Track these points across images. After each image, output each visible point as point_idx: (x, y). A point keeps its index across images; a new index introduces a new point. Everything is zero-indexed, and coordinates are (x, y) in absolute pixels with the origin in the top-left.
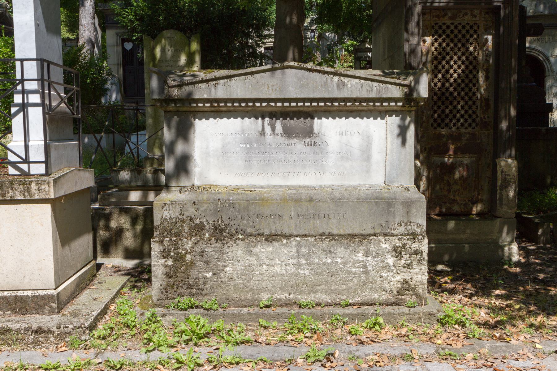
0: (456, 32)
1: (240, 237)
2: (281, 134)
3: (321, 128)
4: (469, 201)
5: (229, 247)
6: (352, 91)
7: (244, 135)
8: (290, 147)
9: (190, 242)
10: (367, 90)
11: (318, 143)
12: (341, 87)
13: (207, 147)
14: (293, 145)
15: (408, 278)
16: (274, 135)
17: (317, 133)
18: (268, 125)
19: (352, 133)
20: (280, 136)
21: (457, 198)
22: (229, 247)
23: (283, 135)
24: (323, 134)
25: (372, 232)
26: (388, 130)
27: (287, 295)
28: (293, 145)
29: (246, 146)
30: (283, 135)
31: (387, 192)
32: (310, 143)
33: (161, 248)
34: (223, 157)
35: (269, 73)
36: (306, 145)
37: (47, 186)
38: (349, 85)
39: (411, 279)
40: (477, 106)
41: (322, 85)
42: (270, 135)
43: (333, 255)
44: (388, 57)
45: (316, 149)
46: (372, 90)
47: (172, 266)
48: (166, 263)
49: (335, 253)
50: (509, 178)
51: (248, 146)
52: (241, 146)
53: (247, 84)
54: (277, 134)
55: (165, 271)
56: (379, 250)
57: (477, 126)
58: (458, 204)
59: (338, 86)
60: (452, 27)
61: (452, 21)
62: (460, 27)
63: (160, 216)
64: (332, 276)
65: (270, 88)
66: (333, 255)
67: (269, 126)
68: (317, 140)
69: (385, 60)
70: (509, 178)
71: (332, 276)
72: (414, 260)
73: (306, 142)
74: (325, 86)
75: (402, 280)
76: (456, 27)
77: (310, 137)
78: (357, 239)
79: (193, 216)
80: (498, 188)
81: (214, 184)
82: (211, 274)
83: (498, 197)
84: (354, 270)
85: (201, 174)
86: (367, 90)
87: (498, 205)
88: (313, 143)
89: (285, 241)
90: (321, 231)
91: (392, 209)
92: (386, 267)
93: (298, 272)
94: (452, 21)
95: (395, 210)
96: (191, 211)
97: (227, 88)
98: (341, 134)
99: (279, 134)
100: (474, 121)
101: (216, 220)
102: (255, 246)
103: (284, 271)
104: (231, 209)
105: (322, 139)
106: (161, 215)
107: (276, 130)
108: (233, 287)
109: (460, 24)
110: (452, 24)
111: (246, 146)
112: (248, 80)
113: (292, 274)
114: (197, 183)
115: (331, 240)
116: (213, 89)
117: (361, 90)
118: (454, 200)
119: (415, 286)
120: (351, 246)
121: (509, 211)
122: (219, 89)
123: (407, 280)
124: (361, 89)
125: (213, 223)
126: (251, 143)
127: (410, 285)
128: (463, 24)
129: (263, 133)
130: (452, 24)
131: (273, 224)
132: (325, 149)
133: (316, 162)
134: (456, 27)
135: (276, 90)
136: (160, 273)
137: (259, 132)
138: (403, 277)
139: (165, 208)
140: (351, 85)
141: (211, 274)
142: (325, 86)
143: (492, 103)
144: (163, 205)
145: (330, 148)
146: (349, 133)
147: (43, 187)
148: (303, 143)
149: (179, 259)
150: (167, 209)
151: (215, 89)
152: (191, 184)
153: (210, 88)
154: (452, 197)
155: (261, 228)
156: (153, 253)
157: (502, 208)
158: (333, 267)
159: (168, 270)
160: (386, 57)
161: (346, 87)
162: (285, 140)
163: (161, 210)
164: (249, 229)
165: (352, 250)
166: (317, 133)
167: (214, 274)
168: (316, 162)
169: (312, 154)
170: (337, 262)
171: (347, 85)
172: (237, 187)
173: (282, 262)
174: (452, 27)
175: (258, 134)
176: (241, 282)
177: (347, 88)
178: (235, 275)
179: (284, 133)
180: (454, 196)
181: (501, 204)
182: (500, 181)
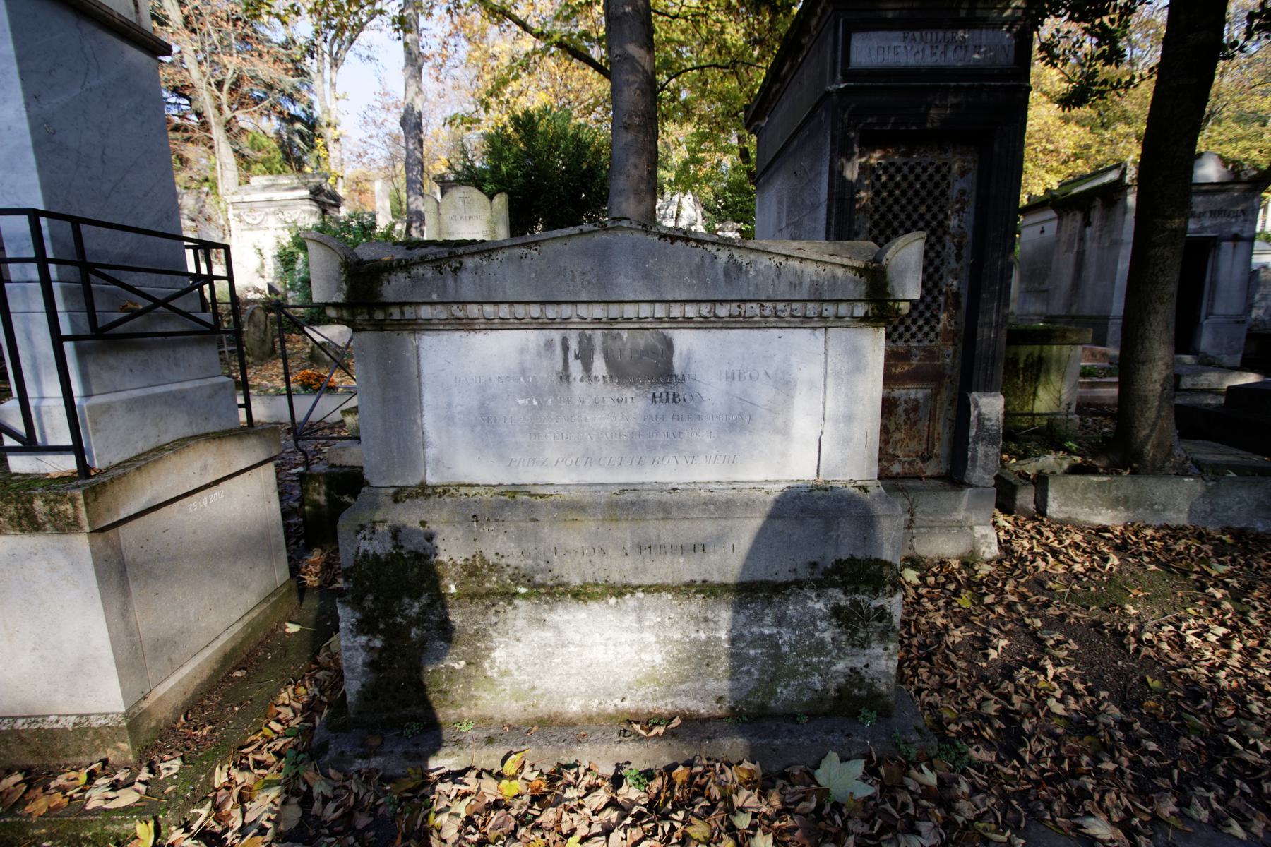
0: (911, 177)
1: (523, 590)
2: (604, 377)
3: (688, 364)
4: (917, 456)
5: (498, 612)
6: (757, 285)
7: (525, 379)
8: (623, 405)
9: (416, 604)
10: (791, 283)
11: (681, 397)
12: (734, 275)
13: (450, 405)
14: (629, 400)
15: (860, 666)
16: (590, 380)
17: (680, 376)
18: (577, 357)
19: (754, 374)
20: (601, 382)
21: (899, 453)
22: (498, 612)
23: (607, 379)
24: (693, 376)
25: (791, 577)
26: (829, 368)
27: (618, 701)
28: (629, 400)
29: (531, 402)
30: (607, 379)
31: (824, 496)
32: (664, 396)
33: (358, 615)
34: (483, 426)
35: (1085, 314)
36: (657, 400)
37: (69, 506)
38: (752, 273)
39: (867, 666)
40: (939, 305)
41: (691, 272)
42: (582, 380)
43: (712, 625)
44: (788, 225)
45: (678, 408)
46: (801, 284)
47: (382, 650)
48: (371, 644)
49: (715, 622)
50: (989, 423)
51: (535, 403)
52: (521, 402)
53: (526, 269)
54: (596, 377)
55: (368, 659)
56: (804, 614)
57: (937, 337)
58: (900, 461)
59: (727, 273)
60: (906, 169)
61: (906, 160)
62: (918, 170)
63: (353, 551)
64: (708, 665)
65: (577, 280)
66: (712, 625)
67: (579, 361)
68: (681, 391)
69: (781, 230)
70: (989, 423)
71: (708, 665)
72: (873, 633)
73: (658, 394)
74: (698, 273)
75: (848, 671)
76: (912, 170)
77: (664, 384)
78: (761, 595)
79: (421, 550)
80: (971, 440)
81: (467, 481)
82: (463, 663)
83: (970, 454)
84: (752, 652)
85: (438, 461)
86: (791, 283)
87: (969, 467)
88: (671, 396)
89: (613, 601)
90: (687, 578)
91: (832, 533)
92: (819, 647)
93: (641, 659)
94: (905, 160)
95: (838, 536)
96: (416, 541)
97: (481, 280)
98: (731, 377)
99: (601, 377)
100: (933, 329)
101: (470, 557)
102: (551, 610)
103: (612, 657)
104: (500, 537)
105: (689, 388)
106: (355, 549)
107: (593, 369)
108: (508, 688)
109: (919, 164)
110: (906, 164)
111: (531, 402)
112: (527, 261)
113: (628, 663)
114: (431, 479)
115: (708, 596)
116: (450, 282)
117: (776, 281)
118: (894, 456)
119: (872, 679)
120: (747, 608)
121: (987, 477)
122: (465, 281)
123: (858, 670)
124: (776, 281)
125: (463, 563)
126: (539, 397)
127: (862, 679)
128: (924, 164)
129: (565, 375)
130: (906, 164)
131: (589, 564)
132: (696, 409)
133: (677, 435)
134: (912, 170)
135: (589, 283)
136: (360, 662)
137: (557, 373)
138: (851, 665)
139: (362, 535)
140: (755, 271)
141: (463, 663)
142: (698, 273)
143: (964, 300)
144: (358, 528)
145: (707, 407)
146: (747, 375)
147: (62, 508)
148: (651, 395)
149: (395, 635)
150: (368, 537)
151: (456, 280)
152: (417, 481)
153: (444, 280)
154: (891, 451)
155: (563, 573)
156: (342, 625)
157: (974, 472)
158: (711, 648)
159: (376, 656)
160: (784, 225)
161: (743, 276)
162: (612, 391)
163: (353, 537)
164: (540, 576)
165: (751, 615)
166: (680, 376)
167: (469, 664)
168: (677, 435)
169: (670, 419)
170: (720, 638)
171: (747, 272)
172: (514, 489)
173: (608, 639)
174: (906, 169)
175: (555, 377)
176: (526, 677)
177: (747, 278)
178: (512, 667)
179: (611, 376)
180: (894, 450)
181: (974, 466)
182: (975, 430)
